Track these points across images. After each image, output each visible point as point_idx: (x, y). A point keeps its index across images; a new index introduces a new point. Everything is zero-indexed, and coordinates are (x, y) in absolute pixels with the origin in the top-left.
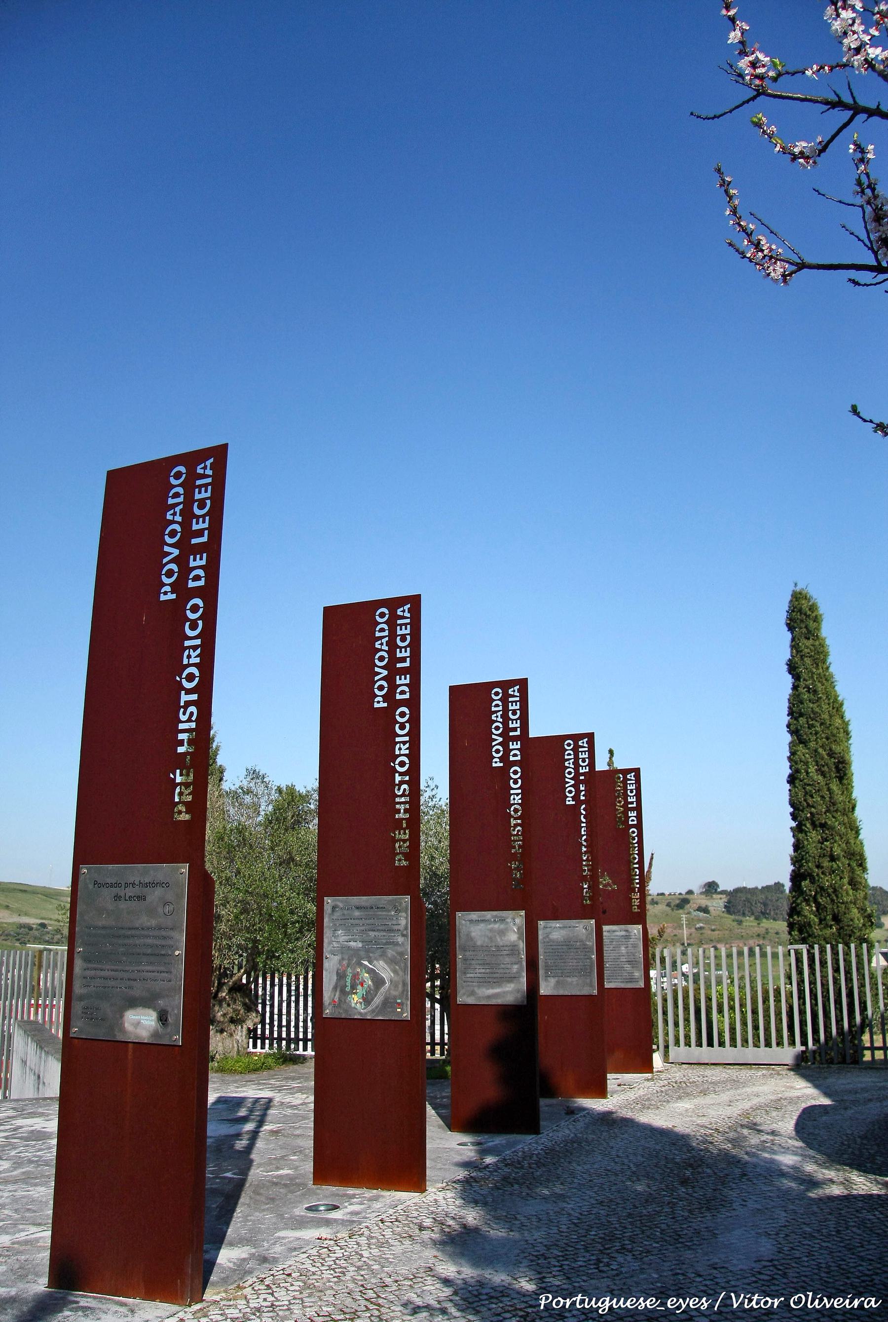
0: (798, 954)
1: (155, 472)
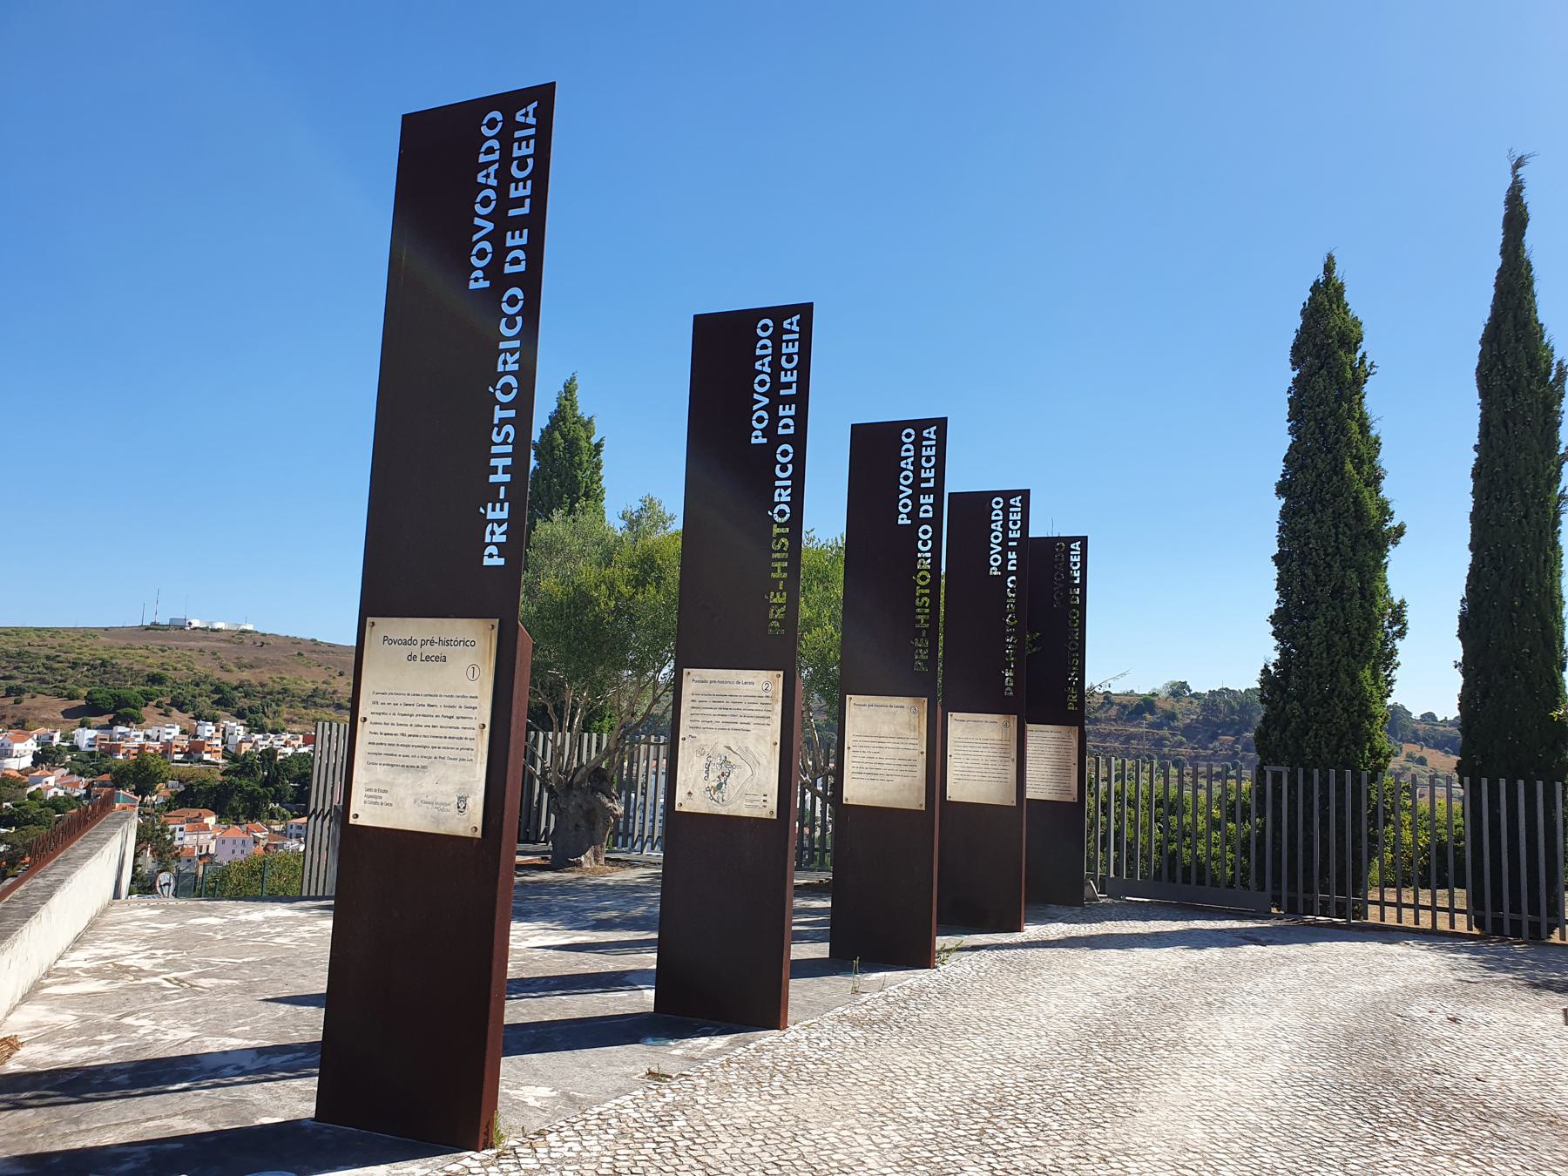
0: (1277, 778)
1: (891, 431)
